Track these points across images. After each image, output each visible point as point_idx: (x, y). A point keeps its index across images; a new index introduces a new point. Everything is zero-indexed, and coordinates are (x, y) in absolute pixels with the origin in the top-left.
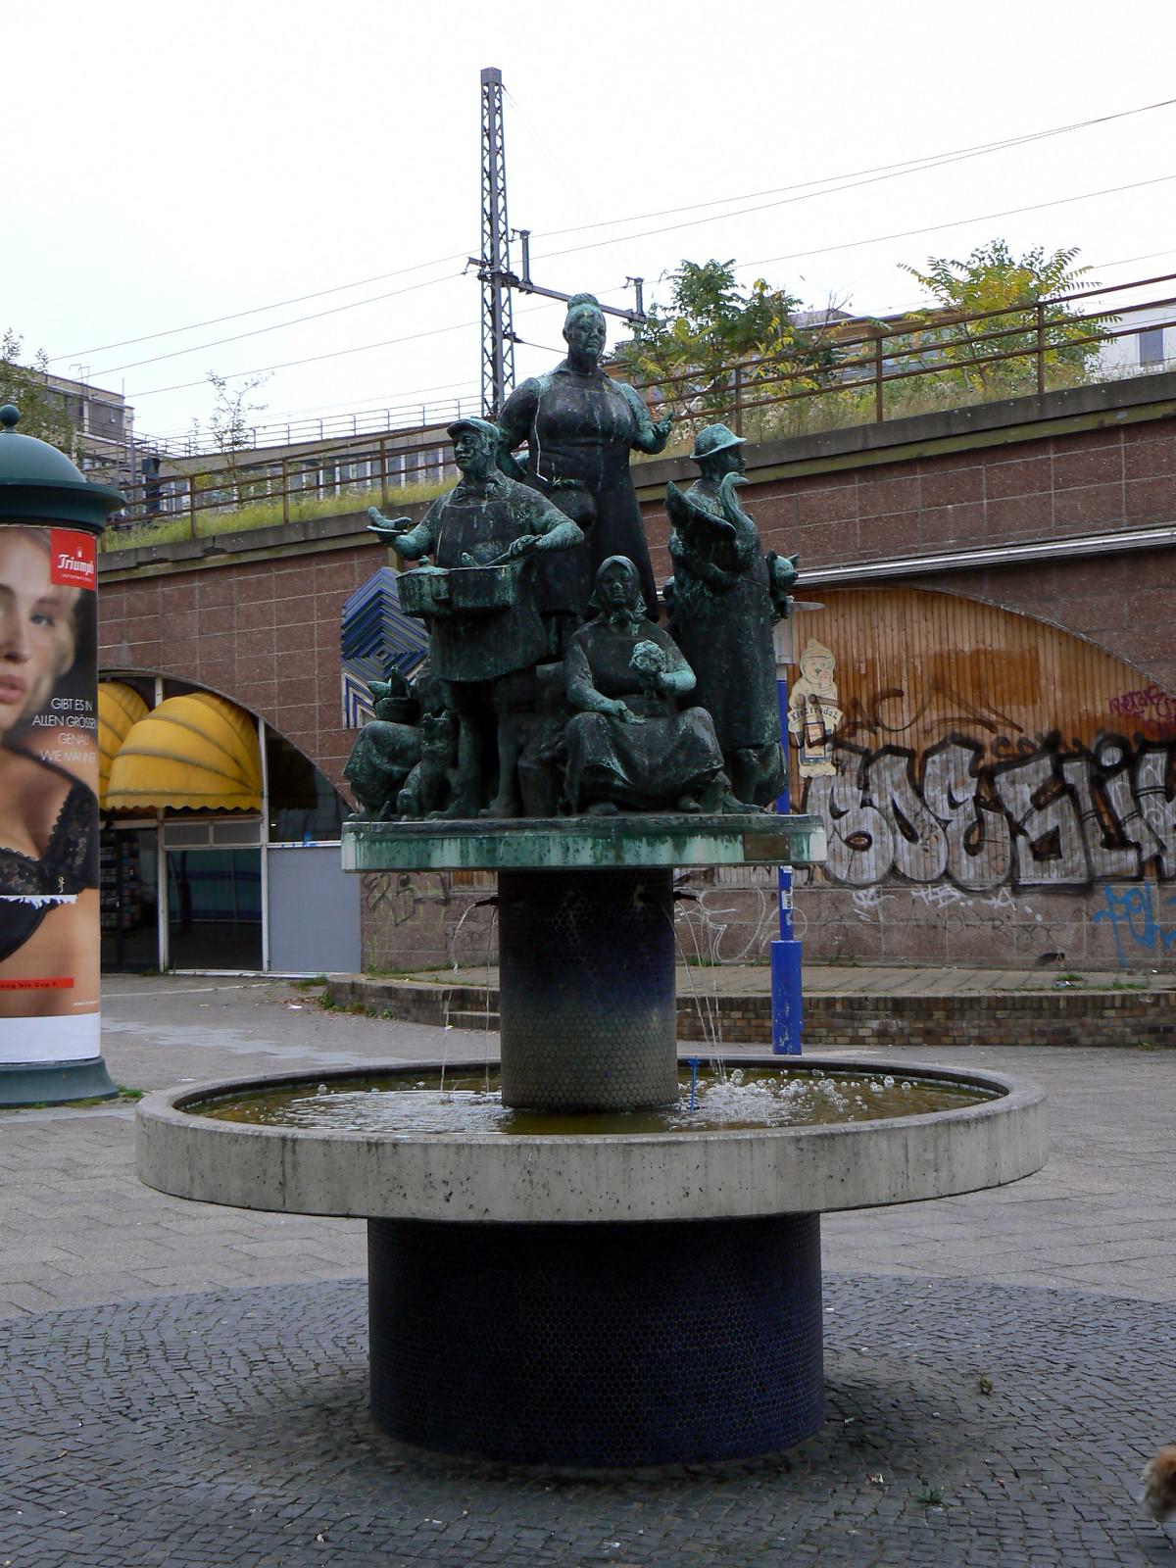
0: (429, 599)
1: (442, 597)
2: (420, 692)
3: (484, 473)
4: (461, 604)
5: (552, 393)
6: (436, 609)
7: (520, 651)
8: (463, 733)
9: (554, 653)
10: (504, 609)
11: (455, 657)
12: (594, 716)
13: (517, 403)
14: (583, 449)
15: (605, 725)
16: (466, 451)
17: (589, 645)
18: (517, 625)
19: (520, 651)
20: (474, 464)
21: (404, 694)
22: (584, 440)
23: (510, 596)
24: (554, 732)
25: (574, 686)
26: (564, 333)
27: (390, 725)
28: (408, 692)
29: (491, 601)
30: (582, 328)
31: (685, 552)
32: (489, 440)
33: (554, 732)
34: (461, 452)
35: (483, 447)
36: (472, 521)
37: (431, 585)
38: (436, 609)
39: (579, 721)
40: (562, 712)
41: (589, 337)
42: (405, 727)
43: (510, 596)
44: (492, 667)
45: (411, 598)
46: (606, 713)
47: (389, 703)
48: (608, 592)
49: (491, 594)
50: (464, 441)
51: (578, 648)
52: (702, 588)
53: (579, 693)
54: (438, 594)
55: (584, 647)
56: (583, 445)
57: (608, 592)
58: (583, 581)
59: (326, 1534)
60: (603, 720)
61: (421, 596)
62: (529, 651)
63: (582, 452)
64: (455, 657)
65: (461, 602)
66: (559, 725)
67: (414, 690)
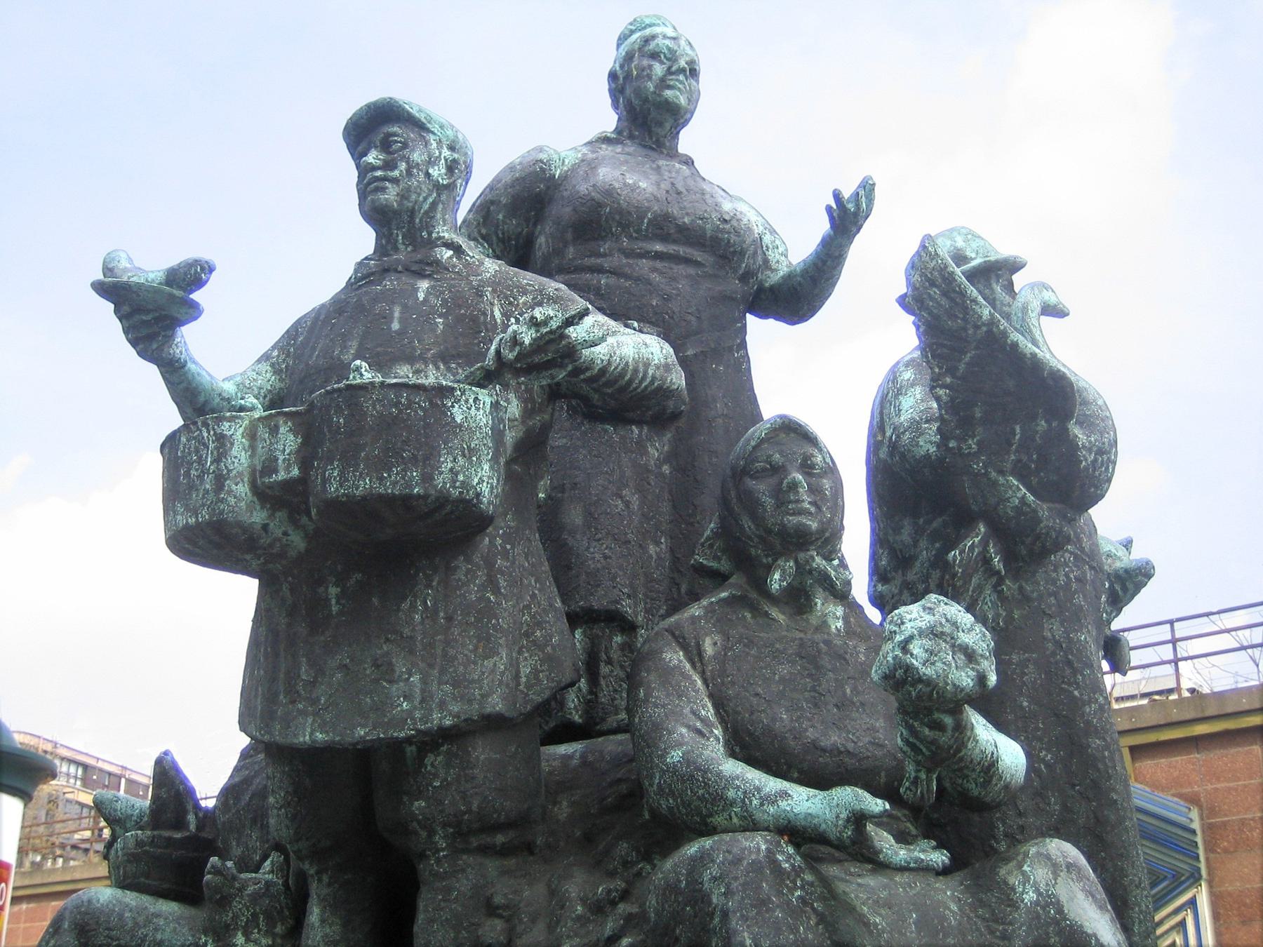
0: (242, 489)
1: (282, 476)
2: (222, 819)
3: (429, 228)
4: (333, 488)
5: (589, 166)
6: (258, 517)
7: (501, 661)
8: (314, 914)
9: (577, 718)
10: (457, 524)
11: (305, 673)
12: (759, 843)
13: (506, 186)
14: (659, 264)
15: (797, 871)
16: (389, 165)
17: (709, 649)
18: (497, 591)
19: (501, 661)
20: (403, 196)
21: (180, 824)
22: (658, 247)
23: (484, 480)
24: (599, 908)
25: (676, 756)
26: (613, 76)
27: (131, 898)
28: (191, 818)
29: (427, 478)
30: (655, 56)
31: (942, 445)
32: (446, 153)
33: (599, 908)
34: (374, 168)
35: (431, 162)
36: (388, 318)
37: (253, 447)
38: (258, 517)
39: (703, 859)
40: (623, 848)
41: (669, 72)
42: (169, 907)
43: (484, 480)
44: (415, 699)
45: (192, 487)
46: (798, 834)
47: (139, 843)
48: (768, 502)
49: (428, 460)
50: (386, 146)
51: (675, 657)
52: (985, 543)
53: (695, 776)
54: (269, 466)
55: (695, 655)
56: (659, 256)
57: (768, 502)
58: (652, 549)
59: (511, 554)
60: (787, 855)
61: (220, 480)
62: (525, 670)
63: (654, 270)
64: (305, 673)
65: (336, 482)
66: (620, 884)
67: (207, 818)
